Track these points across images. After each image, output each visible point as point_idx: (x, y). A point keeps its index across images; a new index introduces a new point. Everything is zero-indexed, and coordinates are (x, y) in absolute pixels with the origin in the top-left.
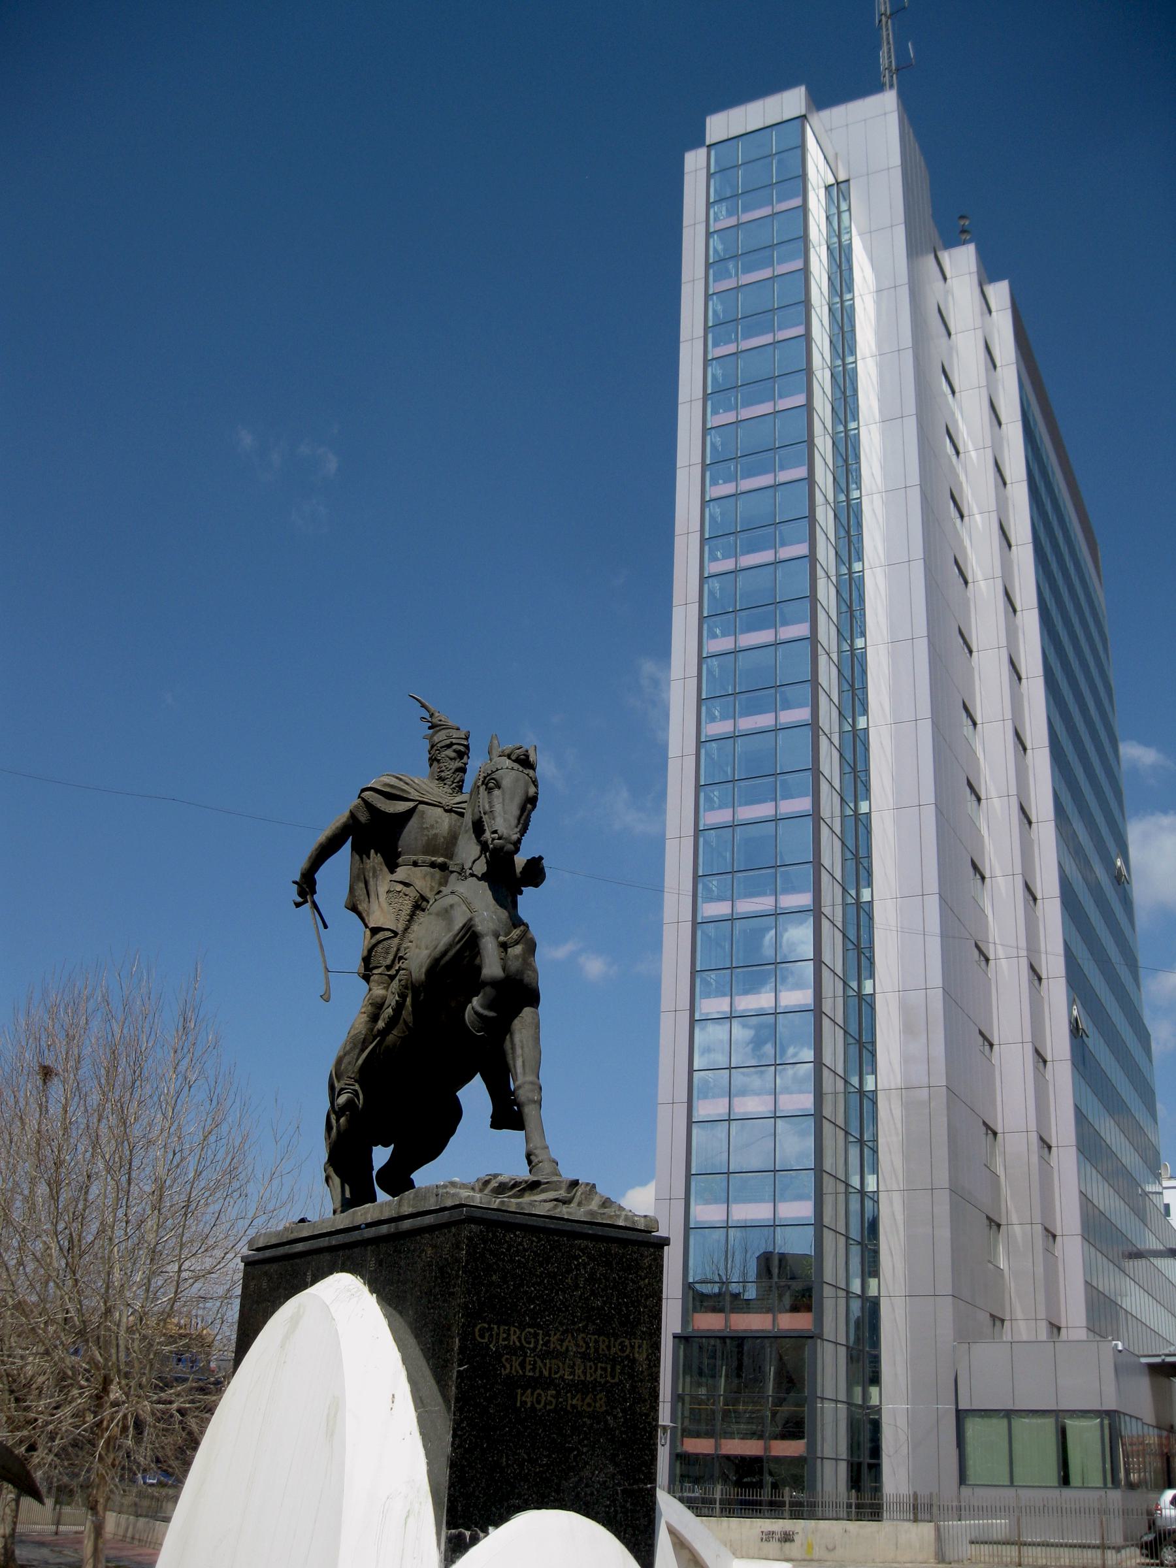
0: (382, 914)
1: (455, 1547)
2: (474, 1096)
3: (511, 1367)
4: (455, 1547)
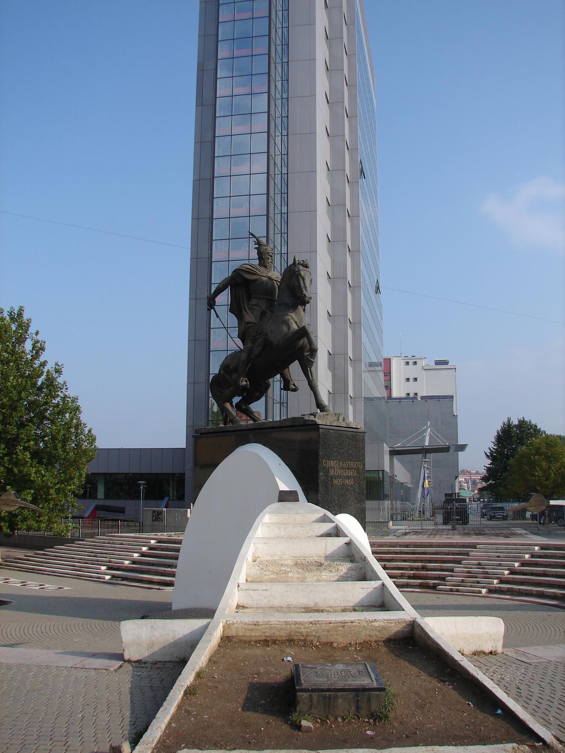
0: (249, 317)
1: (403, 610)
2: (276, 382)
3: (332, 473)
4: (403, 610)
